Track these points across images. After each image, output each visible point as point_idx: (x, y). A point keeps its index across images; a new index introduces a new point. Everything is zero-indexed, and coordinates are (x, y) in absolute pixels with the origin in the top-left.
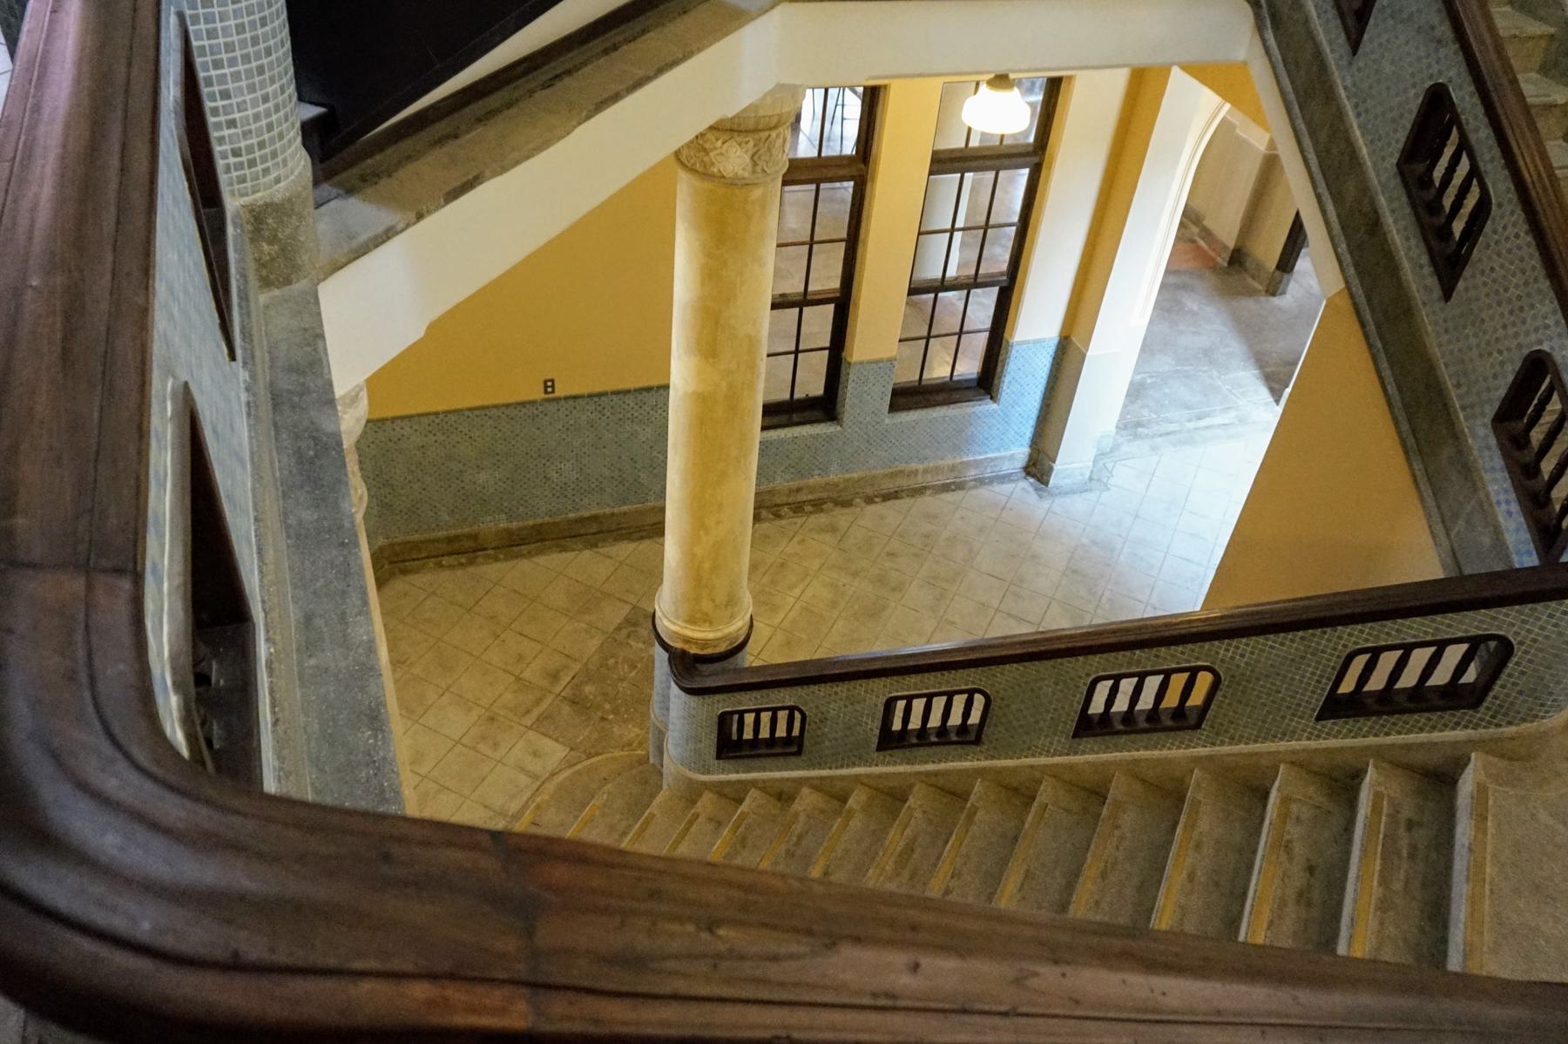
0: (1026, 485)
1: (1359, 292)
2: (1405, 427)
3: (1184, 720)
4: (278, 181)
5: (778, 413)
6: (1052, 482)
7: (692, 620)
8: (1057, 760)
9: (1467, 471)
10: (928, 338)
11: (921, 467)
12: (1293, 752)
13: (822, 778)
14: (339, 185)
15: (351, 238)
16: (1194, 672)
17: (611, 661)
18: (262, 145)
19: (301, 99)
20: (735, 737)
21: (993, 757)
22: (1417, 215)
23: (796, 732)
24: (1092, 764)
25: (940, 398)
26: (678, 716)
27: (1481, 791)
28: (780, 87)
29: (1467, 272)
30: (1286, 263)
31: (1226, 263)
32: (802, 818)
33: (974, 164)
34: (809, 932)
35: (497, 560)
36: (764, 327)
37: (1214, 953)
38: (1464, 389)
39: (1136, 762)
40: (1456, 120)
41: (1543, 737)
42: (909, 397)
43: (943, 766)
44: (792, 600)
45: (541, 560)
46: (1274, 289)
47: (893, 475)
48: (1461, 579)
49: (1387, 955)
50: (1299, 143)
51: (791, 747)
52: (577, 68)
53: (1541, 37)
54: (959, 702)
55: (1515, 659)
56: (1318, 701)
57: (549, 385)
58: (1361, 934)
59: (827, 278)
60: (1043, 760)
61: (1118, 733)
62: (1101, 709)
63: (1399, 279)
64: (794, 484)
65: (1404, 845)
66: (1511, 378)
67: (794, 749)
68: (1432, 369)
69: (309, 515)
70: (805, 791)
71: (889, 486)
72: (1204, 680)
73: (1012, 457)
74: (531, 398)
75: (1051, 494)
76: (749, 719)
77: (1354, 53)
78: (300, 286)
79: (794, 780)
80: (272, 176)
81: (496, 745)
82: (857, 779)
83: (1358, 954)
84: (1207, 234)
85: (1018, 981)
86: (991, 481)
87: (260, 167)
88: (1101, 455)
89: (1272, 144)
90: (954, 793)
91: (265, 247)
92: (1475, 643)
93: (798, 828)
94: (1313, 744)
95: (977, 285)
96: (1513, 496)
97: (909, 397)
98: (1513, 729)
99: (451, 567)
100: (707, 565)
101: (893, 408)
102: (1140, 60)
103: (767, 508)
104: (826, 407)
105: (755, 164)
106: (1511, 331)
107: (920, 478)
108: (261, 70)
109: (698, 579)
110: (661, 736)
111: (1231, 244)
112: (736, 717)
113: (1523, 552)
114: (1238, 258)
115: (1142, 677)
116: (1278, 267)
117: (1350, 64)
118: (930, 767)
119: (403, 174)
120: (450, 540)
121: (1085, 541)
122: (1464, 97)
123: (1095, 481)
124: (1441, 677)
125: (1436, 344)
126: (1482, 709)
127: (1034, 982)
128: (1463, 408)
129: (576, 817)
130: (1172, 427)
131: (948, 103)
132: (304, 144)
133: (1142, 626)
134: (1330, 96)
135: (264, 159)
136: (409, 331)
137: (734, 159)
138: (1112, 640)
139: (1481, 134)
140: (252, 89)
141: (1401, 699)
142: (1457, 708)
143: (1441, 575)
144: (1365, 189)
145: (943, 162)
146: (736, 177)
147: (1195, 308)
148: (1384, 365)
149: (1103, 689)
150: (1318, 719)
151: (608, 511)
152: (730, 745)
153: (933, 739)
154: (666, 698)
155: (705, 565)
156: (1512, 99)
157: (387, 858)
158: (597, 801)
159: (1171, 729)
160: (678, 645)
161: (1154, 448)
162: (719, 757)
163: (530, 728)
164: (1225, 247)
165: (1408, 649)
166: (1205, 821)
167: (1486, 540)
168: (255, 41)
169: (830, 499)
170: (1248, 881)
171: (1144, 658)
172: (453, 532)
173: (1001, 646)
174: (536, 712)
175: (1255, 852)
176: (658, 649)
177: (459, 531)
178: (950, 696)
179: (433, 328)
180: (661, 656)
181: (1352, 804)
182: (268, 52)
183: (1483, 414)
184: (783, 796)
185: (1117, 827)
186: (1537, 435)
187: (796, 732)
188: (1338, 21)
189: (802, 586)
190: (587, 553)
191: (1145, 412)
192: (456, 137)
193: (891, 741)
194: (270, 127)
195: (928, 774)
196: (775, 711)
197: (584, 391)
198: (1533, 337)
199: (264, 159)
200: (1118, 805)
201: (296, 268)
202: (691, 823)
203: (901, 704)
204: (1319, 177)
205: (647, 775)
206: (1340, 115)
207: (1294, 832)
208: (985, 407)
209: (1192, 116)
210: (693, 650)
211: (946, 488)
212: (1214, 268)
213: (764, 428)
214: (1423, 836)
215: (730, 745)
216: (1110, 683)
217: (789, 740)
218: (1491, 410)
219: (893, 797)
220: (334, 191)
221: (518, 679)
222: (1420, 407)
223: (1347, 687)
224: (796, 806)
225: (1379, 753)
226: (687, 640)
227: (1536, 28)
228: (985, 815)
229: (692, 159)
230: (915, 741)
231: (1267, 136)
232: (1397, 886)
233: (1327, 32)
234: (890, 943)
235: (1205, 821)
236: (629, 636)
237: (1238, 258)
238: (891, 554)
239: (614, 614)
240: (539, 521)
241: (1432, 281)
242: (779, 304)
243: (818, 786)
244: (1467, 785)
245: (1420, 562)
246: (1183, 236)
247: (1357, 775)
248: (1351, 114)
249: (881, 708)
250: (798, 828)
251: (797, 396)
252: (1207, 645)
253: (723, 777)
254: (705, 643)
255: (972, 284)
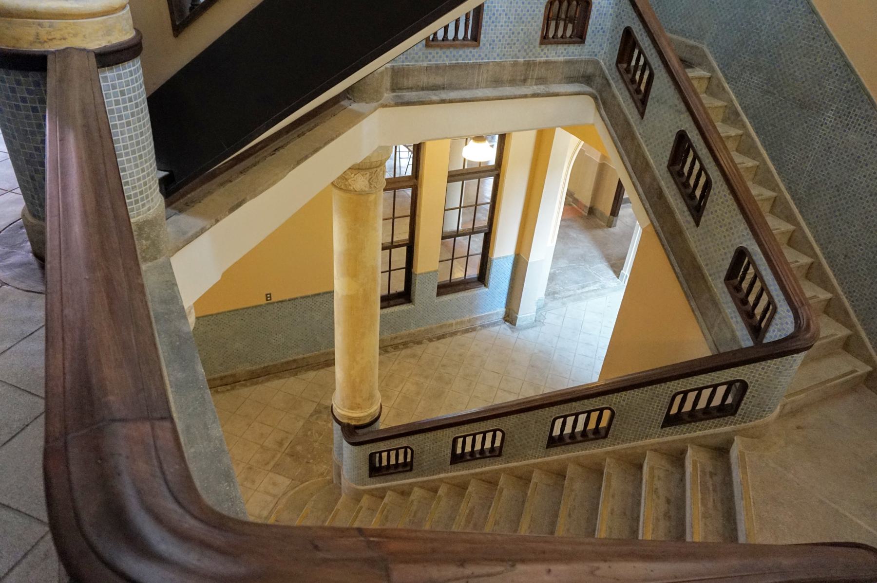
0: (505, 326)
1: (657, 224)
2: (685, 285)
3: (599, 434)
4: (149, 209)
5: (388, 300)
6: (518, 323)
7: (352, 408)
8: (540, 460)
9: (715, 303)
10: (453, 259)
11: (454, 322)
12: (652, 445)
13: (424, 482)
14: (175, 208)
15: (184, 233)
16: (601, 410)
17: (309, 433)
18: (141, 193)
19: (159, 169)
20: (378, 465)
21: (508, 462)
22: (680, 190)
23: (409, 460)
24: (557, 461)
25: (461, 287)
26: (349, 459)
27: (742, 456)
28: (380, 147)
29: (705, 213)
30: (615, 212)
31: (588, 215)
32: (415, 503)
33: (468, 176)
34: (503, 560)
35: (245, 386)
36: (379, 259)
37: (629, 547)
38: (709, 266)
39: (577, 457)
40: (691, 146)
41: (767, 425)
42: (446, 288)
43: (484, 469)
44: (397, 393)
45: (268, 384)
46: (610, 225)
47: (441, 327)
48: (720, 355)
49: (710, 539)
50: (622, 159)
51: (407, 467)
52: (286, 145)
53: (721, 107)
54: (489, 436)
55: (749, 390)
56: (661, 419)
57: (268, 296)
58: (698, 530)
59: (403, 235)
60: (533, 461)
61: (569, 444)
62: (558, 433)
63: (674, 218)
64: (393, 335)
65: (710, 484)
66: (730, 260)
67: (408, 468)
68: (694, 258)
69: (180, 375)
70: (416, 489)
71: (440, 332)
72: (607, 414)
73: (497, 314)
74: (259, 303)
75: (518, 330)
76: (384, 455)
77: (642, 118)
78: (161, 260)
79: (410, 484)
80: (146, 208)
81: (253, 482)
82: (441, 480)
83: (697, 540)
84: (576, 201)
85: (592, 573)
86: (489, 325)
87: (140, 204)
88: (539, 309)
89: (604, 157)
90: (491, 482)
91: (144, 242)
92: (730, 384)
93: (414, 508)
94: (661, 440)
95: (474, 233)
96: (737, 314)
97: (446, 288)
98: (752, 423)
99: (223, 392)
100: (358, 380)
101: (439, 294)
102: (541, 127)
103: (384, 348)
104: (406, 296)
105: (370, 184)
106: (728, 239)
107: (454, 327)
108: (141, 157)
109: (354, 387)
110: (339, 469)
111: (588, 205)
112: (378, 455)
113: (746, 340)
114: (592, 211)
115: (577, 415)
116: (611, 214)
117: (641, 123)
118: (478, 470)
119: (206, 200)
120: (221, 378)
121: (536, 351)
122: (694, 136)
123: (538, 322)
124: (716, 402)
125: (694, 245)
126: (737, 415)
127: (597, 573)
128: (710, 275)
129: (298, 515)
130: (571, 293)
131: (454, 151)
132: (161, 191)
133: (573, 391)
134: (633, 138)
135: (142, 199)
136: (212, 278)
137: (360, 182)
138: (560, 399)
139: (703, 151)
140: (136, 166)
141: (700, 415)
142: (726, 416)
143: (710, 354)
144: (654, 179)
145: (453, 177)
146: (362, 191)
147: (575, 236)
148: (672, 258)
149: (559, 423)
150: (663, 427)
151: (301, 356)
152: (375, 470)
153: (478, 456)
154: (341, 448)
155: (357, 380)
156: (715, 135)
157: (316, 547)
158: (310, 505)
159: (592, 439)
160: (345, 421)
161: (564, 304)
162: (370, 476)
163: (270, 471)
164: (586, 206)
165: (700, 390)
166: (614, 482)
167: (729, 336)
168: (138, 143)
169: (412, 342)
170: (639, 511)
171: (577, 406)
172: (222, 374)
173: (503, 407)
174: (272, 463)
175: (640, 495)
176: (335, 424)
177: (226, 374)
178: (485, 433)
179: (225, 275)
180: (337, 428)
181: (682, 466)
182: (144, 148)
183: (720, 277)
184: (404, 493)
185: (572, 491)
186: (745, 285)
187: (409, 460)
188: (633, 104)
189: (401, 386)
190: (292, 379)
191: (557, 287)
192: (231, 181)
193: (457, 459)
194: (145, 184)
195: (476, 474)
196: (397, 450)
197: (287, 298)
198: (738, 240)
199: (142, 199)
200: (572, 479)
201: (159, 252)
202: (358, 512)
203: (460, 440)
204: (633, 175)
205: (333, 488)
206: (639, 146)
207: (658, 484)
208: (482, 290)
209: (567, 148)
210: (353, 423)
211: (467, 331)
212: (582, 217)
213: (382, 308)
214: (718, 479)
215: (375, 470)
216: (562, 419)
217: (405, 464)
218: (723, 274)
219: (461, 487)
220: (174, 211)
221: (262, 446)
222: (690, 273)
223: (674, 410)
224: (412, 497)
225: (692, 441)
226: (350, 418)
227: (719, 103)
228: (507, 490)
229: (341, 184)
230: (469, 458)
231: (599, 154)
232: (710, 505)
233: (629, 109)
234: (536, 560)
235: (614, 482)
236: (317, 419)
237: (592, 211)
238: (443, 366)
239: (308, 408)
240: (266, 365)
241: (690, 219)
242: (383, 249)
243: (422, 485)
244: (734, 453)
245: (697, 346)
246: (567, 204)
247: (683, 452)
248: (644, 145)
249: (451, 443)
250: (414, 508)
251: (391, 292)
252: (607, 397)
253: (373, 486)
254: (359, 419)
255: (473, 231)
